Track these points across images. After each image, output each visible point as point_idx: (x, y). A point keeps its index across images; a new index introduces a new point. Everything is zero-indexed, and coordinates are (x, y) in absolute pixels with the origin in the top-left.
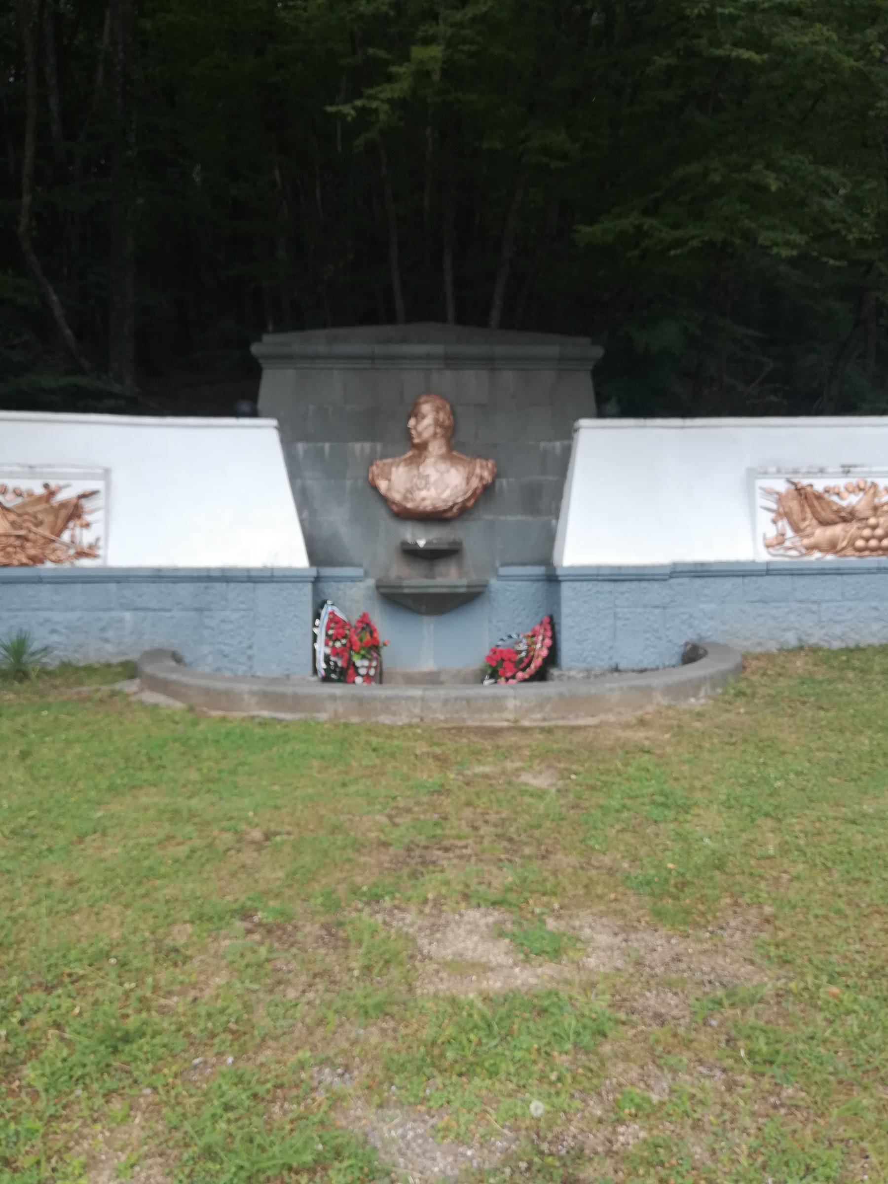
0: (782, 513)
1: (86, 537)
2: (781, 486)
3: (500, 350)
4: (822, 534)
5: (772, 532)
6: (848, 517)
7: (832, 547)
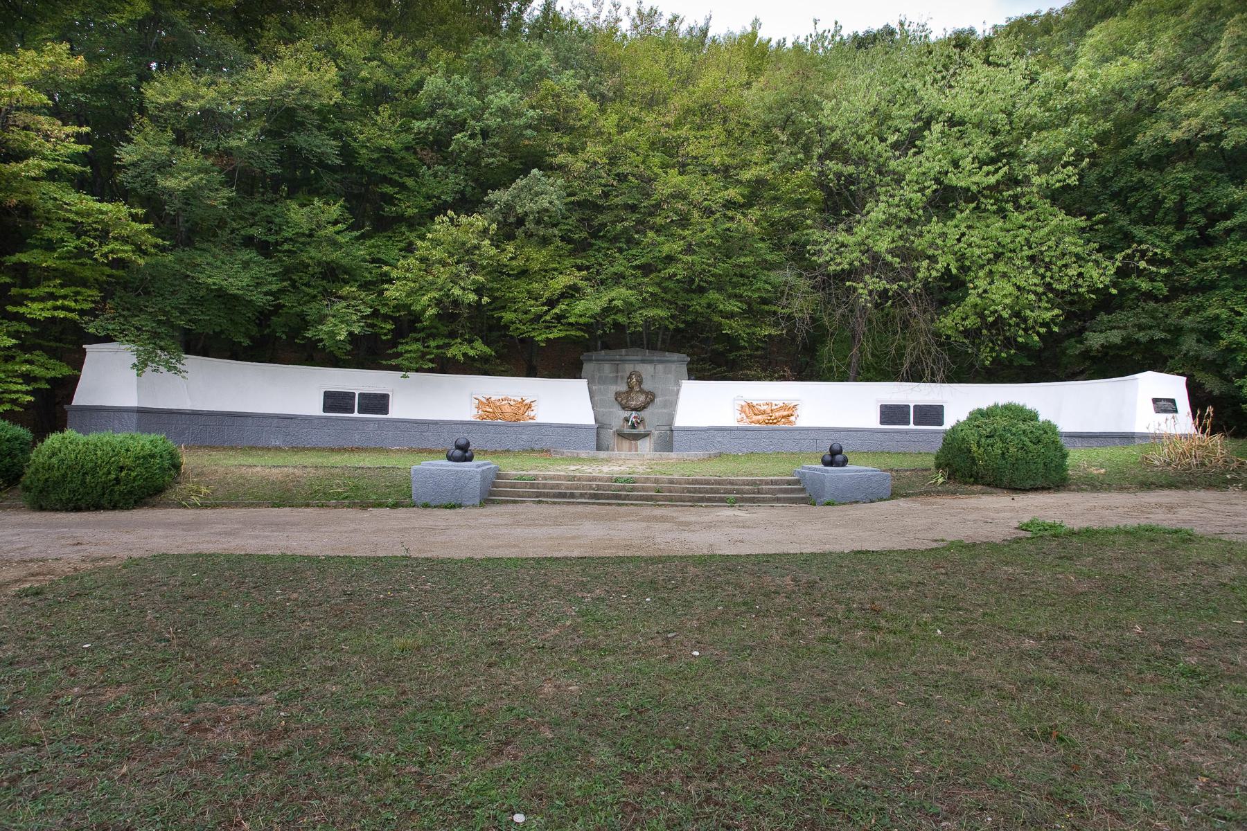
0: (742, 411)
1: (532, 414)
2: (743, 403)
3: (655, 358)
4: (755, 418)
5: (739, 417)
6: (764, 413)
7: (758, 422)
